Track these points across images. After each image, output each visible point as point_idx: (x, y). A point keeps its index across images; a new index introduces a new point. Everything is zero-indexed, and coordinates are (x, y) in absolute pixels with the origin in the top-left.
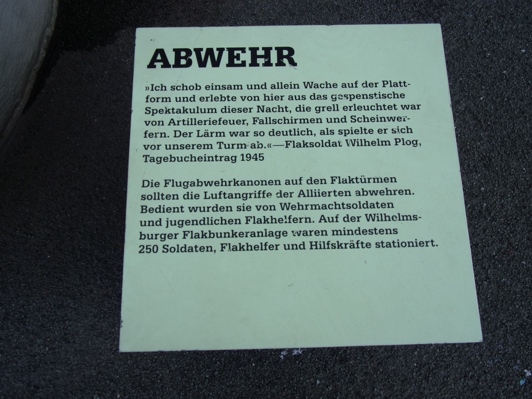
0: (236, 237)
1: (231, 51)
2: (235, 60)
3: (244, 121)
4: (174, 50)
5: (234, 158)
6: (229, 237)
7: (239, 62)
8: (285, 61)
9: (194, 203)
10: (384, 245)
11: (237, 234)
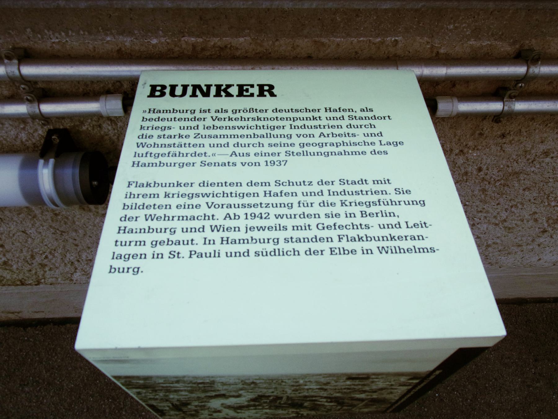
1: (241, 87)
4: (151, 86)
7: (249, 94)
8: (266, 93)
9: (328, 210)
10: (294, 240)
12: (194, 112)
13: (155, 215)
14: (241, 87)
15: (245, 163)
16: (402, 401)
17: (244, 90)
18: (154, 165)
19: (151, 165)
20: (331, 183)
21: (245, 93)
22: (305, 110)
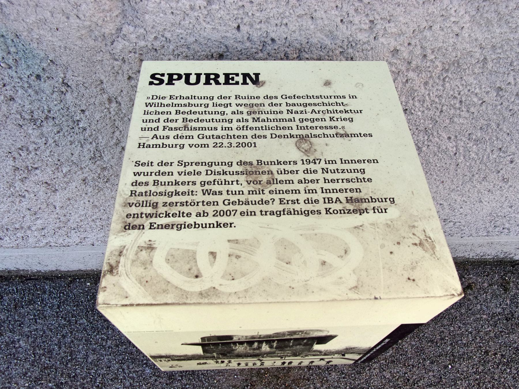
0: (221, 227)
1: (227, 75)
2: (230, 80)
3: (231, 224)
5: (230, 164)
6: (214, 227)
7: (234, 82)
8: (212, 81)
11: (222, 225)
12: (213, 99)
13: (211, 190)
14: (227, 75)
15: (193, 145)
16: (377, 348)
17: (230, 79)
18: (158, 146)
19: (155, 146)
20: (288, 163)
21: (231, 82)
22: (306, 97)
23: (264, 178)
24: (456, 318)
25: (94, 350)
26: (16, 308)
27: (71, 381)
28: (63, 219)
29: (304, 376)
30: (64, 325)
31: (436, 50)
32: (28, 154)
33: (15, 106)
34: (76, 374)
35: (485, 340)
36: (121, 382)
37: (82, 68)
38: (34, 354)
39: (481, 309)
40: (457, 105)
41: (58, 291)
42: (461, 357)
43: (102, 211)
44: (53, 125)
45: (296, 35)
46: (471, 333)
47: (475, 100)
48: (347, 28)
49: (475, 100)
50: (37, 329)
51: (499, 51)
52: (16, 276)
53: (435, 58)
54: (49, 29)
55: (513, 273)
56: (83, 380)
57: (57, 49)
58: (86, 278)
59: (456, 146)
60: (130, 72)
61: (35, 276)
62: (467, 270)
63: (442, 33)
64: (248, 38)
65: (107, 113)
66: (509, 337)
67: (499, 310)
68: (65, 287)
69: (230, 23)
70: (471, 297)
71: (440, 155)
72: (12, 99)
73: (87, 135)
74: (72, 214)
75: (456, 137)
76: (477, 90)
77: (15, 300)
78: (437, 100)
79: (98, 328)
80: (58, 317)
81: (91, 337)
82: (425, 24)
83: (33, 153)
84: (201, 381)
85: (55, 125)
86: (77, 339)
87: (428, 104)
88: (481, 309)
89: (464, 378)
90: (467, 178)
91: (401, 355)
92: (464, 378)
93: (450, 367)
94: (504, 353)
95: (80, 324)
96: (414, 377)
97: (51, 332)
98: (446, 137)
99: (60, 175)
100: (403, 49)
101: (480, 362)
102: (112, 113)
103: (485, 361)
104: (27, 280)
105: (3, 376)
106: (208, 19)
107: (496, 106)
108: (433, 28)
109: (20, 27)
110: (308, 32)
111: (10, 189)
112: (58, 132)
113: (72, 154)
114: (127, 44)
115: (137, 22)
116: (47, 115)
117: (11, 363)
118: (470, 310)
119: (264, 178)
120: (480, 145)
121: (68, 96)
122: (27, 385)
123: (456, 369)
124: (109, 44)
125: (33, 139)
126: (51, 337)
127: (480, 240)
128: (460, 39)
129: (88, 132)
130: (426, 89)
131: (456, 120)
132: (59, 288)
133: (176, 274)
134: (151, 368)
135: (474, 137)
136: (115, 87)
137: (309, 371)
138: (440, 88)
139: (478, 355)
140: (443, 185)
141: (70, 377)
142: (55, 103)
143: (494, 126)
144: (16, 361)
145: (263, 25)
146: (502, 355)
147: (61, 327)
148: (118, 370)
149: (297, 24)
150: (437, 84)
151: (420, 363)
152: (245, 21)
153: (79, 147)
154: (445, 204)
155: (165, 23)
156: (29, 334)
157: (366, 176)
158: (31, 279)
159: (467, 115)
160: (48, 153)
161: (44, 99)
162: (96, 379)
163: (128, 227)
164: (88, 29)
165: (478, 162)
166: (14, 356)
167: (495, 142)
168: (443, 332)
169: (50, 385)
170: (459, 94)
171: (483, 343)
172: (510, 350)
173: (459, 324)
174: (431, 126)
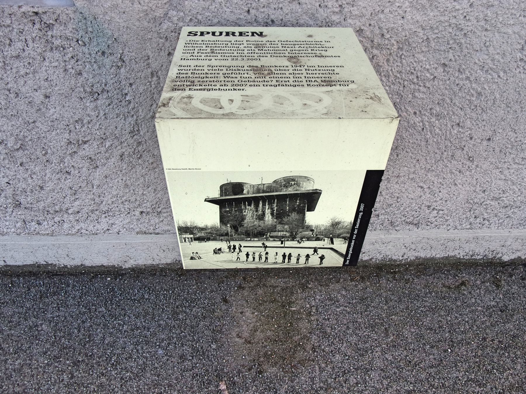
23: (266, 72)
24: (452, 309)
25: (111, 333)
26: (41, 298)
27: (88, 360)
28: (97, 200)
29: (309, 358)
30: (84, 313)
31: (390, 29)
32: (82, 127)
33: (81, 79)
34: (92, 354)
35: (482, 328)
36: (135, 361)
37: (137, 45)
38: (55, 336)
39: (476, 302)
40: (415, 80)
41: (81, 284)
42: (459, 342)
43: (132, 191)
44: (106, 99)
45: (289, 17)
46: (467, 322)
47: (428, 75)
48: (324, 12)
49: (428, 75)
50: (59, 316)
51: (436, 31)
52: (44, 272)
53: (391, 37)
54: (118, 12)
55: (503, 272)
56: (99, 359)
57: (121, 29)
58: (107, 275)
59: (422, 121)
60: (170, 48)
61: (60, 272)
62: (460, 270)
63: (392, 16)
64: (256, 19)
65: (149, 86)
66: (505, 326)
67: (493, 303)
68: (88, 282)
69: (243, 7)
70: (465, 292)
71: (410, 131)
72: (80, 74)
73: (131, 107)
74: (106, 194)
75: (420, 112)
76: (428, 67)
77: (41, 292)
78: (398, 75)
79: (116, 315)
80: (79, 306)
81: (109, 323)
82: (378, 9)
83: (86, 126)
84: (211, 361)
85: (108, 98)
86: (96, 324)
87: (392, 79)
88: (476, 302)
89: (465, 361)
90: (438, 156)
91: (402, 340)
92: (465, 361)
93: (449, 350)
94: (501, 340)
95: (99, 312)
96: (416, 360)
97: (72, 318)
98: (412, 113)
99: (103, 149)
100: (365, 28)
101: (478, 347)
102: (153, 86)
103: (483, 347)
104: (53, 275)
105: (25, 354)
106: (228, 5)
107: (445, 81)
108: (385, 11)
109: (98, 11)
110: (297, 14)
111: (60, 165)
112: (109, 105)
113: (116, 127)
114: (171, 24)
115: (179, 7)
116: (104, 89)
117: (33, 343)
118: (465, 303)
119: (266, 72)
120: (441, 121)
121: (123, 70)
122: (46, 362)
123: (456, 353)
124: (158, 25)
125: (89, 111)
126: (72, 322)
127: (464, 234)
128: (406, 21)
129: (132, 105)
130: (388, 65)
131: (417, 94)
132: (82, 282)
133: (207, 107)
134: (164, 349)
135: (435, 112)
136: (158, 62)
137: (314, 353)
138: (399, 64)
139: (476, 340)
140: (419, 164)
141: (87, 356)
142: (112, 76)
143: (448, 101)
144: (37, 342)
145: (265, 9)
146: (499, 341)
147: (81, 314)
148: (132, 351)
149: (289, 8)
150: (397, 61)
151: (420, 347)
152: (253, 5)
153: (122, 121)
154: (425, 186)
155: (198, 8)
156: (51, 319)
157: (335, 72)
158: (57, 275)
159: (424, 90)
160: (97, 127)
161: (104, 73)
162: (111, 358)
163: (174, 90)
164: (145, 13)
165: (443, 138)
166: (36, 337)
167: (453, 117)
168: (440, 321)
169: (68, 362)
170: (415, 70)
171: (480, 331)
172: (506, 337)
173: (456, 315)
174: (398, 100)
